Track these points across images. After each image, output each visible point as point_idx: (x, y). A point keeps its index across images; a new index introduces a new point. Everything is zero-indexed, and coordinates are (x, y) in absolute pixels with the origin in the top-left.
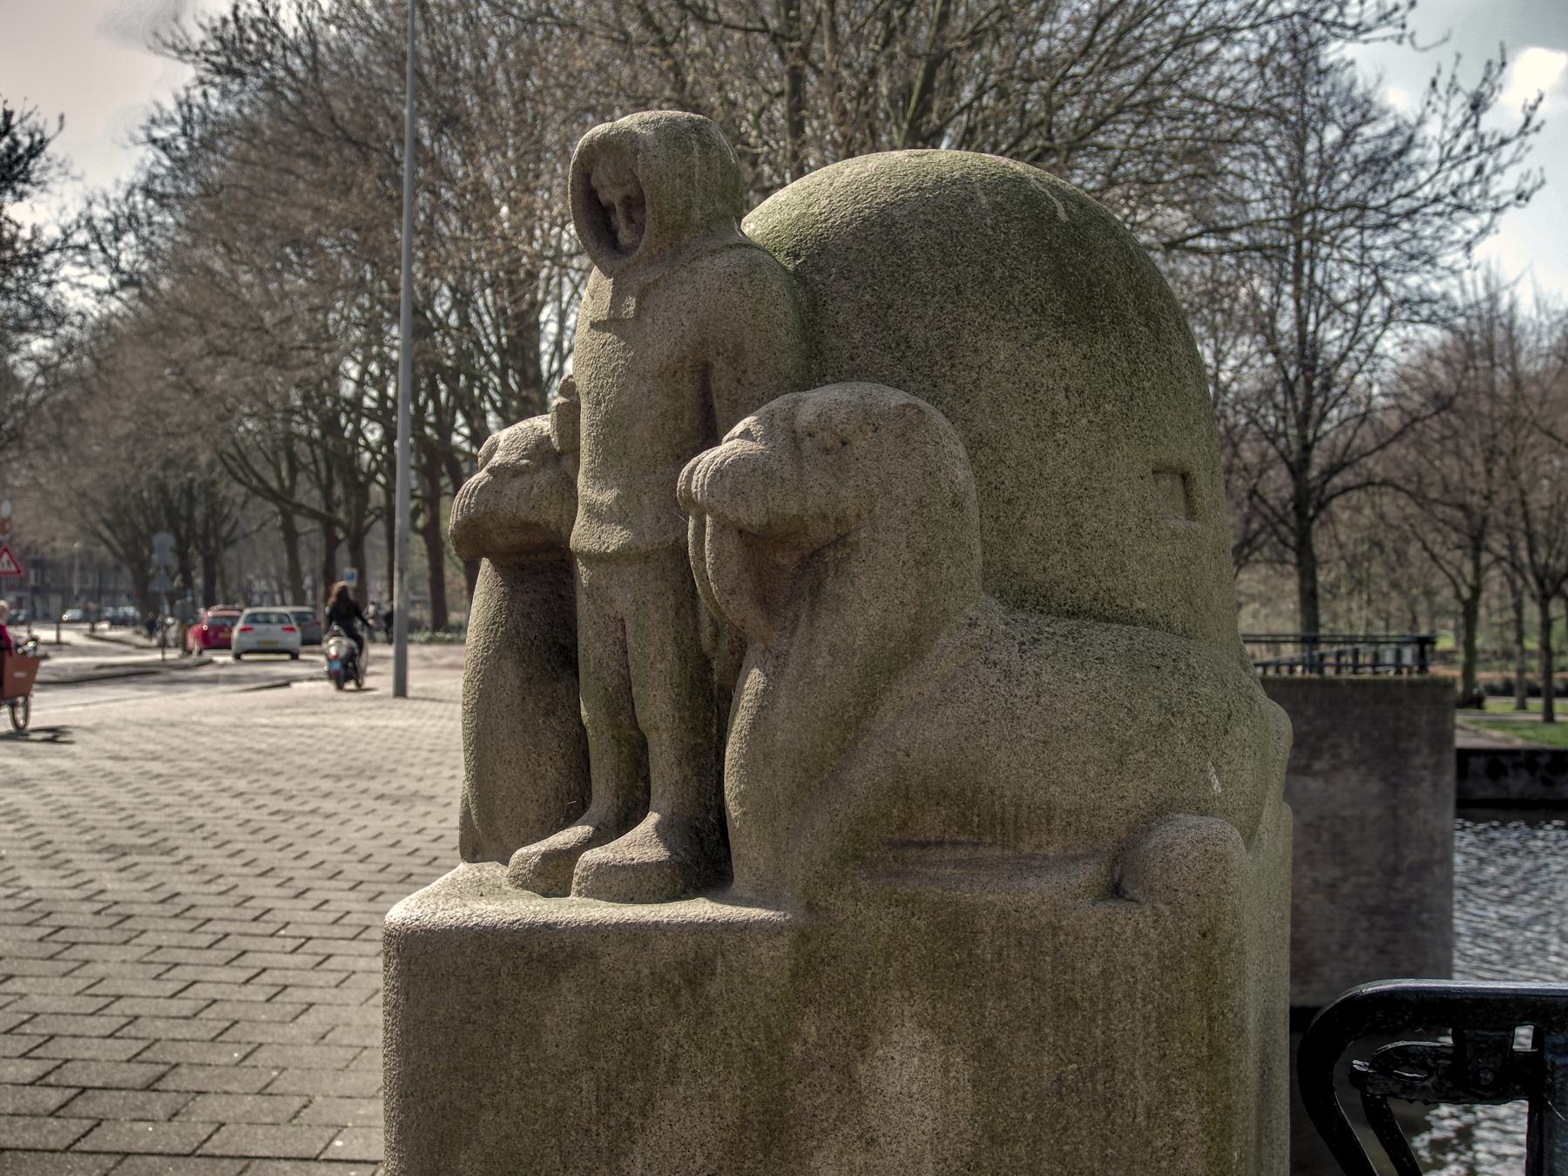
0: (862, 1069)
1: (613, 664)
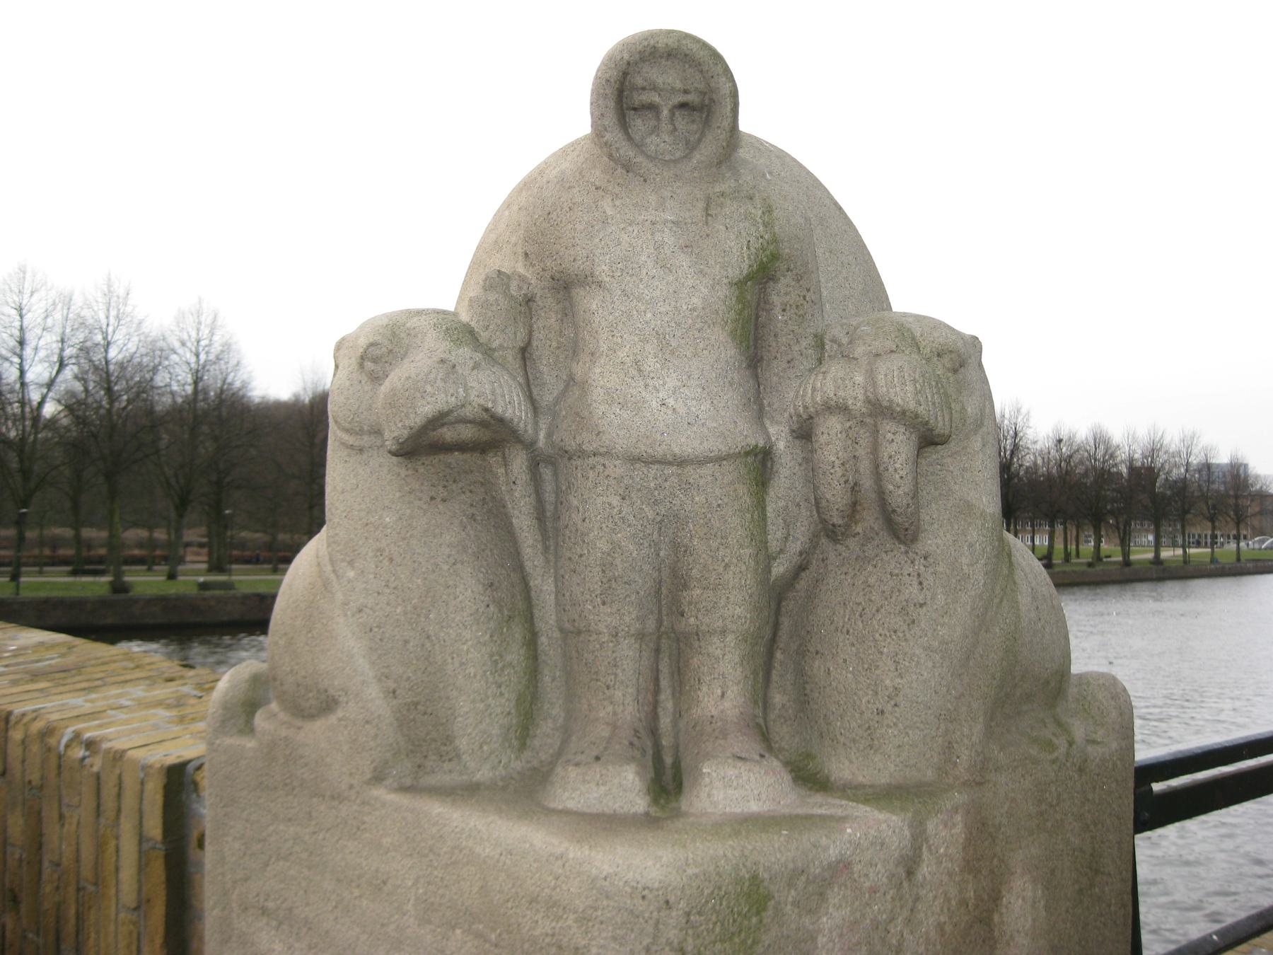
0: (996, 918)
1: (646, 567)
